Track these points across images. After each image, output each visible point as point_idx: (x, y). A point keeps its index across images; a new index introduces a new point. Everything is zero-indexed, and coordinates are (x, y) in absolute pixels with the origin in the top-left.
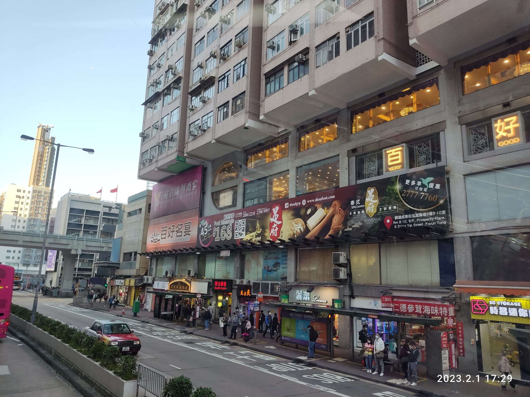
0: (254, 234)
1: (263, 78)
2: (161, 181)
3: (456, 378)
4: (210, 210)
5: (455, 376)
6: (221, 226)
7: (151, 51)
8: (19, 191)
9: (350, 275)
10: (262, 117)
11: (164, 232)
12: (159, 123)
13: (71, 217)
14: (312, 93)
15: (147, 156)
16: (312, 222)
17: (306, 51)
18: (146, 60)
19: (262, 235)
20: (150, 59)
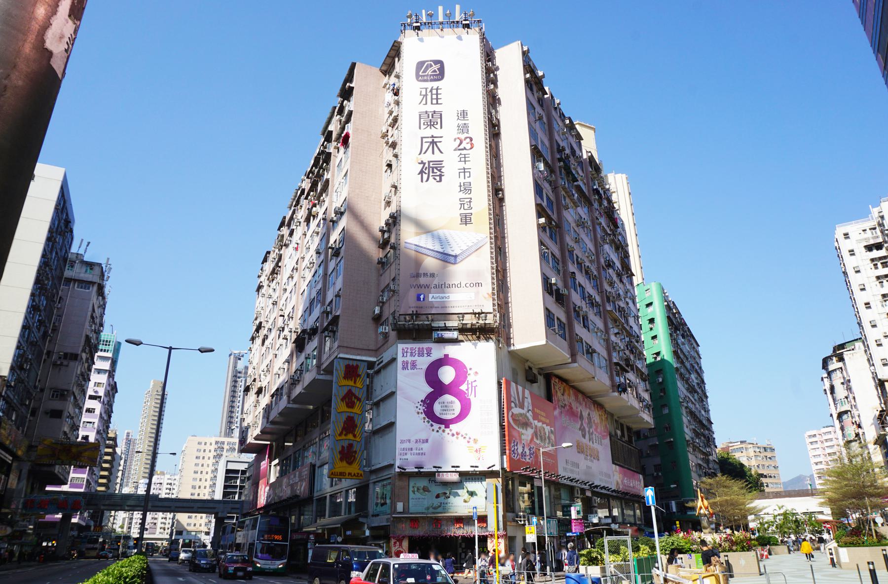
8: (200, 443)
13: (227, 479)
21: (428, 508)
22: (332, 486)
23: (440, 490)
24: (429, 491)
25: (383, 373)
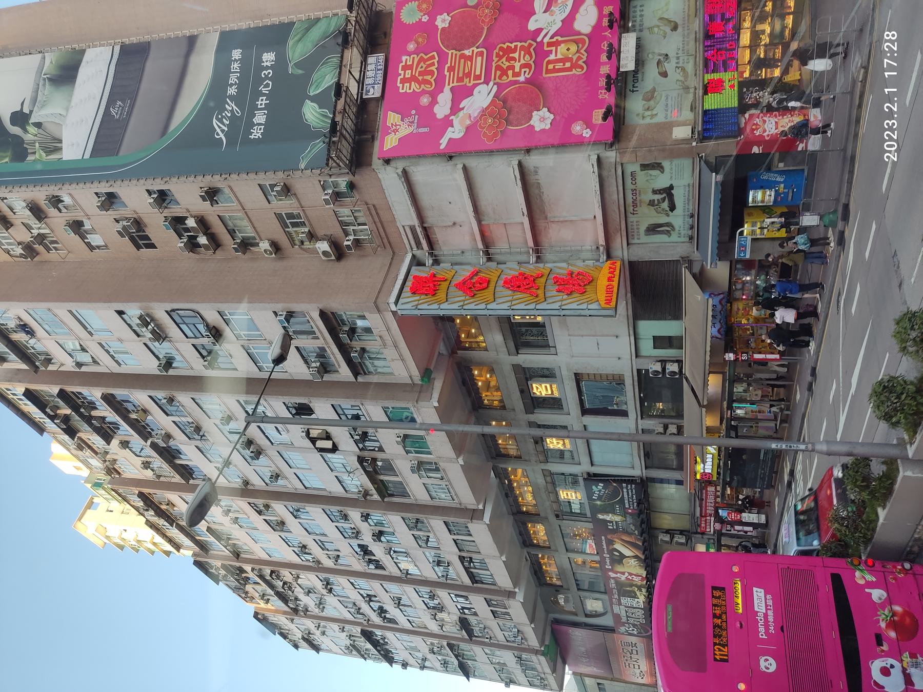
0: (638, 593)
1: (475, 585)
2: (564, 662)
3: (891, 129)
4: (607, 621)
5: (887, 130)
6: (627, 617)
7: (403, 665)
9: (682, 532)
11: (632, 666)
12: (497, 667)
14: (504, 558)
15: (537, 682)
16: (627, 552)
17: (462, 559)
18: (413, 671)
19: (640, 589)
20: (411, 666)
21: (687, 88)
22: (624, 414)
23: (651, 72)
24: (654, 90)
25: (432, 219)
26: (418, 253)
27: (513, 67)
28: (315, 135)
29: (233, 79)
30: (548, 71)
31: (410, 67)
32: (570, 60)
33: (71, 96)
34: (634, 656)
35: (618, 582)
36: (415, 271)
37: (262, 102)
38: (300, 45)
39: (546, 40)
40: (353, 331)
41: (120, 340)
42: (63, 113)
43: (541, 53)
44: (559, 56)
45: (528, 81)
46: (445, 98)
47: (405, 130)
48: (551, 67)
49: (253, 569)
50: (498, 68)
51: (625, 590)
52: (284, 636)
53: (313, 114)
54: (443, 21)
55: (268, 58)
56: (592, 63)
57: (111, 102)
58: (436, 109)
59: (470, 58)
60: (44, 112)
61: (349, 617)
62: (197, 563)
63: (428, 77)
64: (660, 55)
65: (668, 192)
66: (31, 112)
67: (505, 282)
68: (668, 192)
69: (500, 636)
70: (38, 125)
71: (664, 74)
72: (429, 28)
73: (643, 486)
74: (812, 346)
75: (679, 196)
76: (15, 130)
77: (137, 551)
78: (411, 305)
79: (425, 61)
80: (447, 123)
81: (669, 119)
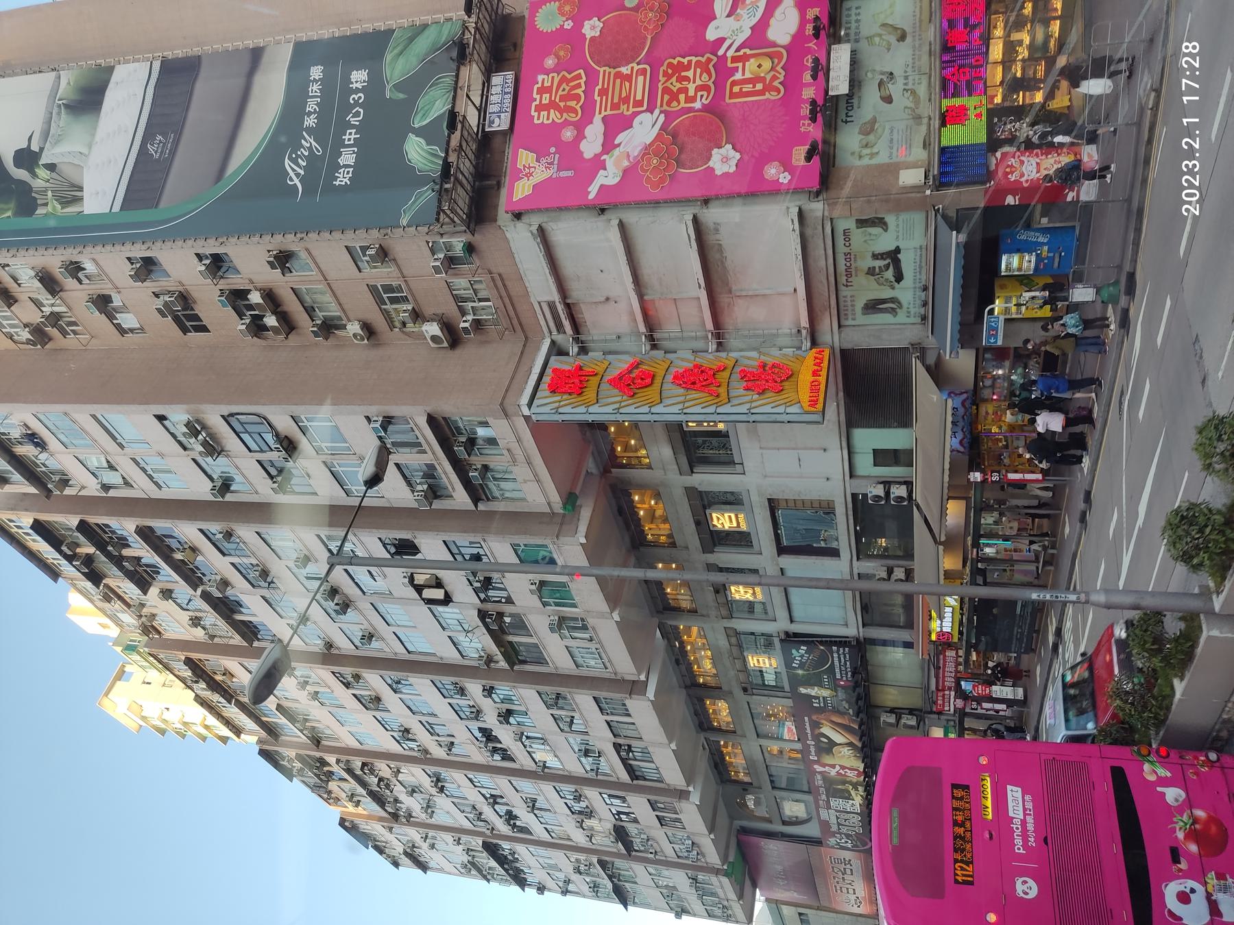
0: (853, 793)
1: (635, 782)
2: (755, 885)
3: (1191, 172)
4: (812, 830)
5: (1185, 174)
6: (839, 824)
7: (539, 889)
9: (911, 711)
10: (643, 678)
11: (844, 890)
12: (664, 891)
14: (673, 746)
15: (718, 912)
16: (838, 738)
17: (617, 747)
18: (552, 897)
19: (855, 787)
20: (549, 890)
21: (918, 118)
22: (834, 553)
23: (871, 97)
24: (874, 121)
25: (577, 293)
26: (559, 338)
27: (686, 90)
28: (421, 180)
29: (312, 105)
30: (732, 95)
31: (548, 90)
32: (762, 80)
33: (95, 129)
34: (848, 877)
35: (826, 778)
36: (555, 362)
37: (350, 136)
38: (401, 61)
39: (730, 54)
40: (472, 442)
41: (161, 455)
42: (85, 151)
43: (723, 71)
44: (748, 75)
45: (705, 108)
46: (595, 131)
47: (541, 174)
48: (736, 89)
49: (338, 761)
50: (666, 90)
51: (836, 789)
52: (380, 850)
53: (418, 152)
54: (592, 28)
55: (359, 77)
56: (792, 84)
57: (148, 137)
58: (584, 146)
59: (628, 78)
60: (58, 150)
61: (467, 825)
62: (263, 753)
63: (572, 103)
64: (882, 73)
65: (893, 256)
66: (42, 149)
67: (676, 377)
68: (893, 256)
69: (668, 850)
70: (51, 167)
71: (888, 100)
72: (573, 37)
73: (860, 649)
74: (1086, 462)
75: (908, 262)
76: (21, 174)
77: (184, 736)
78: (550, 407)
79: (568, 81)
80: (598, 164)
81: (895, 160)
